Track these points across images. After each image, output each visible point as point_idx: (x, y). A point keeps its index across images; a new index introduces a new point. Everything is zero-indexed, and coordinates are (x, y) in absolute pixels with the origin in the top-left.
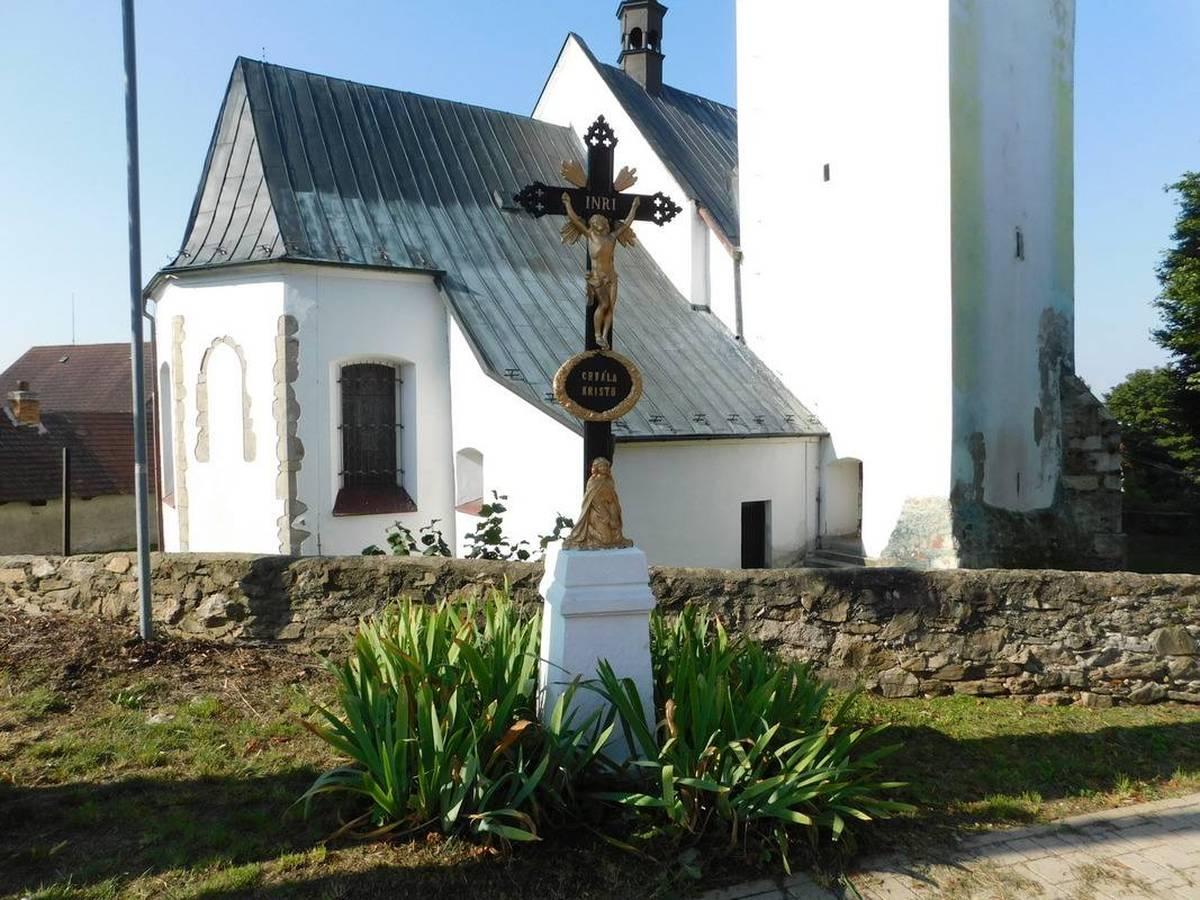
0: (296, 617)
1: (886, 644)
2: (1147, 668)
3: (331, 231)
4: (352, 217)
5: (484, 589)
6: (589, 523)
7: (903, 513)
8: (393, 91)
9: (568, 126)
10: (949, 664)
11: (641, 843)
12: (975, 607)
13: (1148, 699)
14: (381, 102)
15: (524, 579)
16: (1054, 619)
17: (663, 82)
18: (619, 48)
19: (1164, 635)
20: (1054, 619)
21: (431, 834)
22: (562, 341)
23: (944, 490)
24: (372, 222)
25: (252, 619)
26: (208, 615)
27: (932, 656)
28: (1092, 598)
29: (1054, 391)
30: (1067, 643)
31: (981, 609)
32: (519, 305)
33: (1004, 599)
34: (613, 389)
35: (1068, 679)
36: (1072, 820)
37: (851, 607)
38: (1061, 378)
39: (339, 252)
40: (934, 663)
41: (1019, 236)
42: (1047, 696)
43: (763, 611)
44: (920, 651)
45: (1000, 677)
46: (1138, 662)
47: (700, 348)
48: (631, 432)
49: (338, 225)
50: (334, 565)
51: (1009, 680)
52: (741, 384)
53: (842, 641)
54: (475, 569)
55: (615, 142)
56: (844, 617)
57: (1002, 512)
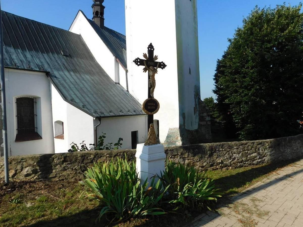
0: (54, 171)
1: (195, 161)
2: (240, 160)
3: (12, 58)
4: (18, 55)
5: (106, 158)
6: (150, 139)
7: (169, 132)
8: (28, 19)
9: (79, 34)
10: (207, 164)
11: (176, 211)
12: (211, 151)
13: (241, 167)
14: (24, 22)
15: (116, 154)
16: (225, 152)
17: (104, 26)
18: (92, 16)
19: (242, 153)
20: (225, 152)
21: (131, 219)
22: (84, 92)
23: (178, 126)
24: (25, 57)
25: (40, 173)
26: (25, 173)
27: (204, 163)
28: (231, 147)
29: (197, 103)
30: (227, 157)
31: (212, 152)
32: (71, 82)
33: (216, 149)
34: (154, 107)
35: (228, 164)
36: (243, 191)
37: (188, 154)
38: (198, 100)
39: (15, 65)
40: (204, 164)
41: (190, 69)
42: (224, 168)
43: (171, 156)
44: (202, 162)
45: (216, 166)
46: (238, 159)
47: (118, 93)
48: (105, 115)
49: (14, 57)
50: (65, 155)
51: (218, 166)
52: (129, 102)
53: (187, 162)
54: (103, 153)
55: (154, 49)
56: (187, 156)
57: (189, 131)
